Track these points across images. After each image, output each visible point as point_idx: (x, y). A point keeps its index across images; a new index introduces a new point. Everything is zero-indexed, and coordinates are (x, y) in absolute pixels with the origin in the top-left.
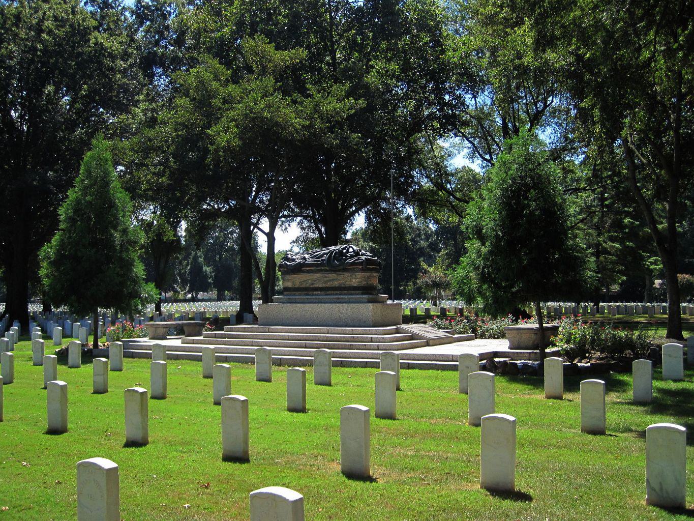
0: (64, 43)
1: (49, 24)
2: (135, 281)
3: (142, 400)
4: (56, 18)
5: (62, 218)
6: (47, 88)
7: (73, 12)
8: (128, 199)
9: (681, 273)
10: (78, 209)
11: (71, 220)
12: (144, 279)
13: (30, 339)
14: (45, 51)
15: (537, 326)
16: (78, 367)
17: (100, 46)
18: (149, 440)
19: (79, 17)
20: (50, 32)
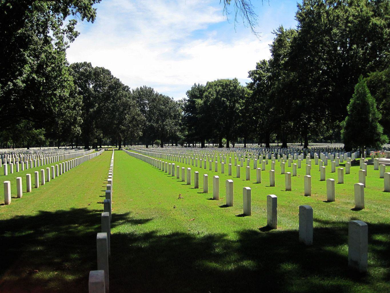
0: (358, 26)
1: (351, 18)
2: (378, 135)
3: (342, 172)
4: (353, 15)
5: (348, 110)
6: (353, 46)
7: (361, 11)
8: (374, 101)
9: (247, 144)
10: (354, 105)
11: (351, 111)
12: (382, 133)
13: (359, 165)
14: (350, 31)
15: (196, 144)
16: (338, 166)
17: (375, 25)
18: (353, 186)
19: (364, 13)
20: (351, 22)
